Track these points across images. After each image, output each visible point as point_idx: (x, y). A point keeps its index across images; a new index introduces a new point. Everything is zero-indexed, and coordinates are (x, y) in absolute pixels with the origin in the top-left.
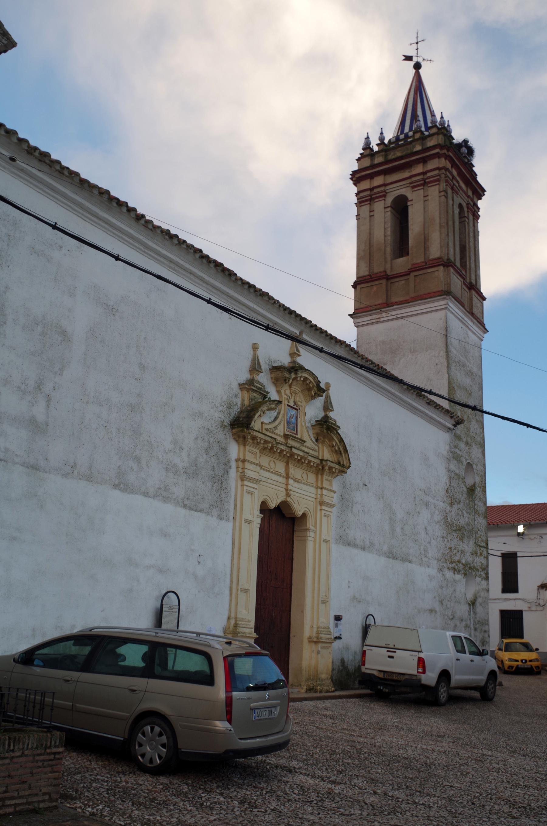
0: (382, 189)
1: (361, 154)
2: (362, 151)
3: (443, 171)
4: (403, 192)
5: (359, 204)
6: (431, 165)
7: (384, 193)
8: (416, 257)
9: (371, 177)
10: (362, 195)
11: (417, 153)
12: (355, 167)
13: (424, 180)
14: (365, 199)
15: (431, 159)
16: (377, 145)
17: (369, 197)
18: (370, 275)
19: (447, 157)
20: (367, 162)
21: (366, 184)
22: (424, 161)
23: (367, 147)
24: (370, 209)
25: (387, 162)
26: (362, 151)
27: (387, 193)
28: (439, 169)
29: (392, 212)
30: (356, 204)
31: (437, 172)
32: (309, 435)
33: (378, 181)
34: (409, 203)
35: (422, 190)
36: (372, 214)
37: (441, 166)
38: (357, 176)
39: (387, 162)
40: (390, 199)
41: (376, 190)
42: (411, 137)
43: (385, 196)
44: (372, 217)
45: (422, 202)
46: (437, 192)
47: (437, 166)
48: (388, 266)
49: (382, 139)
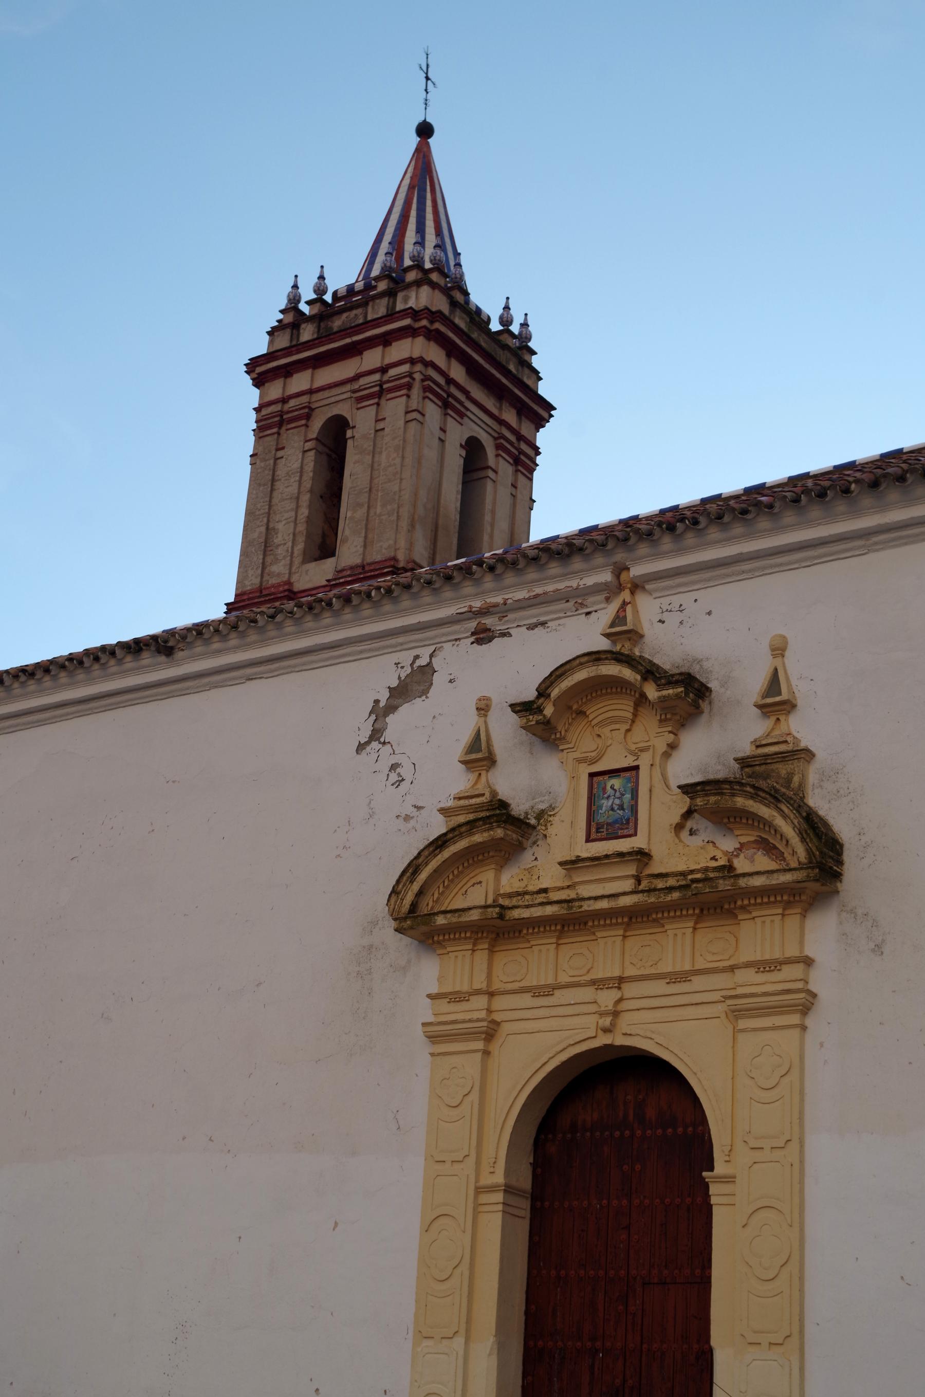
0: (304, 399)
1: (278, 321)
2: (281, 316)
3: (419, 367)
4: (343, 410)
5: (261, 430)
6: (402, 349)
7: (306, 410)
8: (350, 552)
9: (287, 372)
10: (264, 412)
11: (376, 322)
12: (261, 347)
13: (281, 414)
14: (271, 423)
15: (298, 371)
16: (309, 303)
17: (377, 389)
18: (260, 590)
19: (433, 336)
20: (283, 341)
21: (275, 390)
22: (386, 340)
23: (292, 306)
24: (407, 407)
25: (392, 315)
26: (281, 316)
27: (312, 410)
28: (412, 361)
29: (318, 453)
30: (254, 430)
31: (405, 368)
32: (758, 873)
33: (300, 382)
34: (349, 433)
35: (303, 428)
36: (381, 425)
37: (416, 355)
38: (259, 369)
39: (329, 336)
40: (317, 424)
41: (392, 372)
42: (359, 292)
43: (308, 417)
44: (380, 433)
45: (401, 423)
46: (403, 413)
47: (406, 355)
48: (402, 543)
49: (320, 290)
